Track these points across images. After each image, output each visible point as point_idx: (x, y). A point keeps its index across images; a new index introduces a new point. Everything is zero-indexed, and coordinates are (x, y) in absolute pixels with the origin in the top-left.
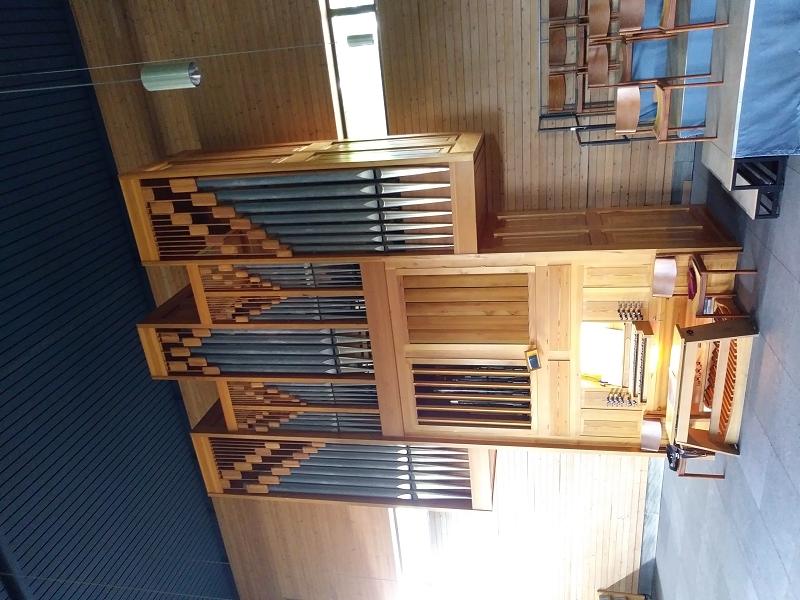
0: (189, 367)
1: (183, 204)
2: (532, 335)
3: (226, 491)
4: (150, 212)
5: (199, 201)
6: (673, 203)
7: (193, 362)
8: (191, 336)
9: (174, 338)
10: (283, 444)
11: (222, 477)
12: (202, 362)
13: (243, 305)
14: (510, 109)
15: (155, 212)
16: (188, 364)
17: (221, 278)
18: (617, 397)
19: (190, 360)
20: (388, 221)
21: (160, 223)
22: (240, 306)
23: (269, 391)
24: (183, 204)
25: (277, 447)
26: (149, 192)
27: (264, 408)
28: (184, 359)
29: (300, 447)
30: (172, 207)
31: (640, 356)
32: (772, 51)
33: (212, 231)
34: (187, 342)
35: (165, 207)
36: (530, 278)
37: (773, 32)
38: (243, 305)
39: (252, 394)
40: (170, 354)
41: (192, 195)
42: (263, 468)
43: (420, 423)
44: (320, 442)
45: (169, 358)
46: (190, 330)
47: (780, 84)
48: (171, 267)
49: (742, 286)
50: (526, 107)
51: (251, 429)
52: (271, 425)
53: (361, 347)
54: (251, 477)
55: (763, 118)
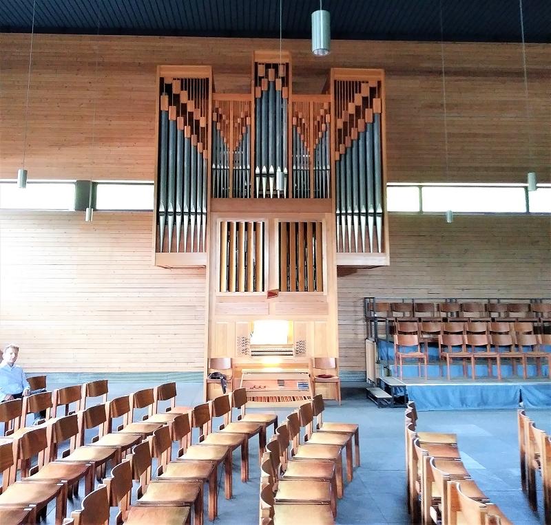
0: (261, 78)
1: (367, 102)
2: (283, 293)
3: (162, 80)
4: (363, 82)
5: (368, 112)
6: (298, 353)
7: (264, 81)
8: (283, 86)
9: (281, 73)
10: (205, 129)
11: (174, 79)
12: (265, 88)
13: (304, 124)
14: (370, 282)
15: (362, 84)
16: (263, 77)
17: (322, 114)
18: (245, 341)
19: (266, 80)
20: (346, 217)
21: (355, 86)
22: (303, 122)
23: (244, 128)
24: (367, 102)
25: (202, 124)
26: (375, 85)
27: (232, 122)
28: (267, 76)
29: (203, 142)
30: (366, 96)
31: (286, 353)
32: (450, 394)
33: (351, 115)
34: (279, 82)
35: (365, 92)
36: (320, 293)
37: (457, 394)
38: (304, 124)
39: (242, 116)
40: (270, 68)
41: (371, 110)
42: (182, 110)
43: (280, 223)
44: (207, 154)
45: (268, 66)
46: (287, 85)
47: (437, 399)
48: (155, 101)
49: (367, 402)
50: (371, 290)
51: (215, 110)
52: (219, 124)
53: (274, 190)
54: (175, 100)
55: (425, 396)
